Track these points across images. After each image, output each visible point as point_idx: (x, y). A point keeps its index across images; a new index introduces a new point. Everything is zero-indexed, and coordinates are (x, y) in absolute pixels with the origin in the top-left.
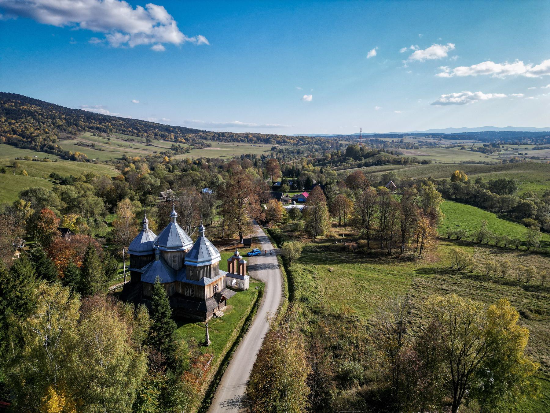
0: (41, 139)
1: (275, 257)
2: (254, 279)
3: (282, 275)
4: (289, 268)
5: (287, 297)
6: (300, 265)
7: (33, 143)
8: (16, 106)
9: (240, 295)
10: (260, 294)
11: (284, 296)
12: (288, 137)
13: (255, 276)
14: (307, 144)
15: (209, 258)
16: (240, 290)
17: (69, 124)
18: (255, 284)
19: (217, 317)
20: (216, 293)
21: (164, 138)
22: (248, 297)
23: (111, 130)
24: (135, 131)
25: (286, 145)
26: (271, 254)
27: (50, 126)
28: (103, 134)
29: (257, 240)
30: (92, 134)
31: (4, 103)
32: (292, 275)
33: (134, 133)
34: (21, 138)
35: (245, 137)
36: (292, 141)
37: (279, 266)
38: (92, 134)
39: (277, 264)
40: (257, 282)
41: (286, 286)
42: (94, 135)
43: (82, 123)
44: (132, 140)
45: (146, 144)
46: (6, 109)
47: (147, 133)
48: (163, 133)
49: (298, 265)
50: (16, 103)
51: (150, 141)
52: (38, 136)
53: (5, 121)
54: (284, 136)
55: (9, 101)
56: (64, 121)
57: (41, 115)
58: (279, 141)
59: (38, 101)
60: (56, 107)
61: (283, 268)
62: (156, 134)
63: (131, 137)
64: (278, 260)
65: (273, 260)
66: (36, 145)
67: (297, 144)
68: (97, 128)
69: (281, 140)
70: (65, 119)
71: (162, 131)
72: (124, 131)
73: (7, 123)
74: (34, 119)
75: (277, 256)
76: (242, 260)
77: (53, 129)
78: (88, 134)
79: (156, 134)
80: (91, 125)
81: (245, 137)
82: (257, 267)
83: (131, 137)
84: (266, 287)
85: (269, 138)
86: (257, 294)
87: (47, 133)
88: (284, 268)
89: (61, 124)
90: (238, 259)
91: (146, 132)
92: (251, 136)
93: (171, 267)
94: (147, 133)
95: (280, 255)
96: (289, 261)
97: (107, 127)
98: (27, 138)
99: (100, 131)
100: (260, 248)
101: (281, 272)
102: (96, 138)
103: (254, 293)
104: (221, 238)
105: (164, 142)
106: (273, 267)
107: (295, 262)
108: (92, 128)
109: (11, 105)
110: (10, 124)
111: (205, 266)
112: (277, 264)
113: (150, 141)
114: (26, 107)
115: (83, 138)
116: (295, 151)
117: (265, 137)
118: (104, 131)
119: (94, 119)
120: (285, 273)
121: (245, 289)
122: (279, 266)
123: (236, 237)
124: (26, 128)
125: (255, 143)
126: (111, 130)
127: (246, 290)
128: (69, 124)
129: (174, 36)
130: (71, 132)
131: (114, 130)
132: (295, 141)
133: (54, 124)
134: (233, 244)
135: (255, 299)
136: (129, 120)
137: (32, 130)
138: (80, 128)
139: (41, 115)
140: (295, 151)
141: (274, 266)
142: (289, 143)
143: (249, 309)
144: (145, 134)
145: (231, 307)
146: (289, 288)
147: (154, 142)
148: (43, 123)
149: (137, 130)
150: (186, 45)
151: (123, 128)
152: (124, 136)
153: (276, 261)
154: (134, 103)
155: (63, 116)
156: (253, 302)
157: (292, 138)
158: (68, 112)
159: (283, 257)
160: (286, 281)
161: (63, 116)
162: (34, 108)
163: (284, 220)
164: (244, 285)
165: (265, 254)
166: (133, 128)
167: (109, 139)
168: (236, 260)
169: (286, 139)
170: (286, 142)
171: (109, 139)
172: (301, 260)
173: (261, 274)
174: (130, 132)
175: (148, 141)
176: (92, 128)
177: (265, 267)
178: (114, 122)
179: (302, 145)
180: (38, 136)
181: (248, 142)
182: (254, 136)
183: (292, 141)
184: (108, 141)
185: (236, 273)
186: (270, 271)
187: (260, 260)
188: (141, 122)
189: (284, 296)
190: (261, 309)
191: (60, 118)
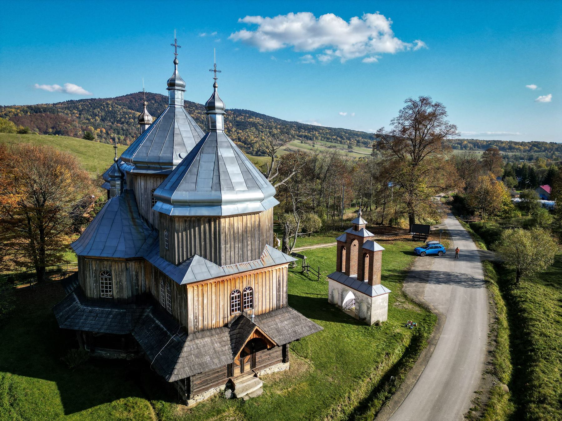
0: (258, 145)
1: (479, 264)
2: (412, 301)
3: (492, 306)
4: (515, 292)
5: (507, 376)
6: (549, 290)
7: (251, 148)
8: (245, 119)
9: (351, 335)
10: (415, 348)
11: (492, 370)
12: (516, 143)
13: (417, 293)
14: (544, 151)
15: (213, 195)
16: (360, 320)
17: (282, 132)
18: (409, 314)
19: (234, 396)
20: (241, 317)
21: (366, 144)
22: (375, 345)
23: (317, 138)
24: (339, 139)
25: (512, 152)
26: (469, 257)
27: (266, 135)
28: (309, 142)
29: (446, 234)
30: (300, 141)
31: (237, 117)
32: (524, 310)
33: (338, 140)
34: (243, 144)
35: (458, 144)
36: (522, 148)
37: (486, 282)
38: (300, 141)
39: (482, 277)
40: (417, 309)
41: (505, 337)
42: (302, 143)
43: (293, 132)
44: (335, 147)
45: (347, 151)
46: (237, 122)
47: (350, 140)
48: (366, 140)
49: (541, 289)
50: (245, 116)
51: (351, 148)
52: (256, 143)
53: (235, 131)
54: (511, 142)
55: (240, 115)
56: (279, 130)
57: (262, 125)
58: (504, 147)
59: (263, 115)
60: (276, 120)
61: (496, 290)
62: (358, 142)
63: (334, 144)
64: (485, 270)
65: (474, 270)
66: (253, 150)
67: (529, 151)
68: (306, 137)
69: (507, 147)
70: (280, 128)
71: (365, 138)
72: (328, 139)
73: (236, 133)
74: (256, 129)
75: (483, 262)
76: (371, 243)
77: (269, 137)
78: (296, 142)
79: (358, 142)
80: (301, 133)
81: (458, 144)
82: (428, 276)
83: (334, 144)
84: (439, 329)
85: (490, 144)
86: (407, 342)
87: (263, 140)
88: (501, 290)
89: (276, 132)
90: (361, 239)
91: (349, 139)
92: (466, 142)
93: (147, 221)
94: (350, 140)
95: (492, 262)
96: (514, 275)
97: (314, 135)
98: (248, 144)
99: (307, 139)
100: (447, 245)
101: (491, 296)
102: (303, 145)
103: (397, 337)
104: (380, 224)
105: (366, 149)
106: (470, 282)
107: (531, 280)
108: (301, 136)
109: (242, 119)
110: (238, 133)
111: (198, 220)
112: (482, 277)
113: (351, 148)
114: (251, 120)
115: (291, 145)
116: (526, 157)
117: (485, 143)
118: (311, 139)
119: (304, 129)
120: (502, 303)
121: (373, 320)
122: (486, 282)
123: (405, 223)
124: (248, 136)
125: (470, 149)
126: (317, 138)
127: (377, 324)
128: (282, 132)
129: (390, 45)
130: (282, 140)
131: (320, 138)
132: (527, 148)
133: (270, 133)
134: (396, 235)
135: (394, 359)
136: (335, 129)
137: (253, 137)
138: (290, 136)
139: (262, 125)
140: (526, 157)
141: (473, 280)
142: (517, 149)
143: (362, 391)
144: (348, 141)
145: (304, 369)
146: (513, 345)
147: (356, 149)
148: (262, 132)
149: (341, 137)
150: (399, 56)
151: (328, 136)
152: (328, 143)
153: (481, 271)
154: (341, 115)
155: (279, 126)
156: (384, 367)
157: (523, 144)
158: (284, 123)
159: (499, 266)
160: (505, 323)
161: (279, 126)
162: (257, 120)
163: (505, 212)
164: (369, 308)
165: (456, 256)
166: (338, 136)
167: (313, 146)
168: (356, 242)
169: (513, 145)
170: (514, 148)
171: (313, 146)
172: (546, 278)
173: (432, 294)
174: (334, 139)
175: (350, 147)
176: (301, 136)
177: (448, 279)
178: (321, 131)
179: (536, 151)
180: (256, 143)
181: (462, 149)
182: (469, 143)
183: (522, 148)
184: (313, 148)
185: (354, 275)
186: (460, 290)
187: (440, 265)
188: (346, 131)
189: (494, 373)
190: (406, 395)
191: (276, 128)
